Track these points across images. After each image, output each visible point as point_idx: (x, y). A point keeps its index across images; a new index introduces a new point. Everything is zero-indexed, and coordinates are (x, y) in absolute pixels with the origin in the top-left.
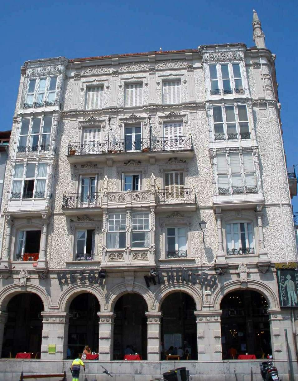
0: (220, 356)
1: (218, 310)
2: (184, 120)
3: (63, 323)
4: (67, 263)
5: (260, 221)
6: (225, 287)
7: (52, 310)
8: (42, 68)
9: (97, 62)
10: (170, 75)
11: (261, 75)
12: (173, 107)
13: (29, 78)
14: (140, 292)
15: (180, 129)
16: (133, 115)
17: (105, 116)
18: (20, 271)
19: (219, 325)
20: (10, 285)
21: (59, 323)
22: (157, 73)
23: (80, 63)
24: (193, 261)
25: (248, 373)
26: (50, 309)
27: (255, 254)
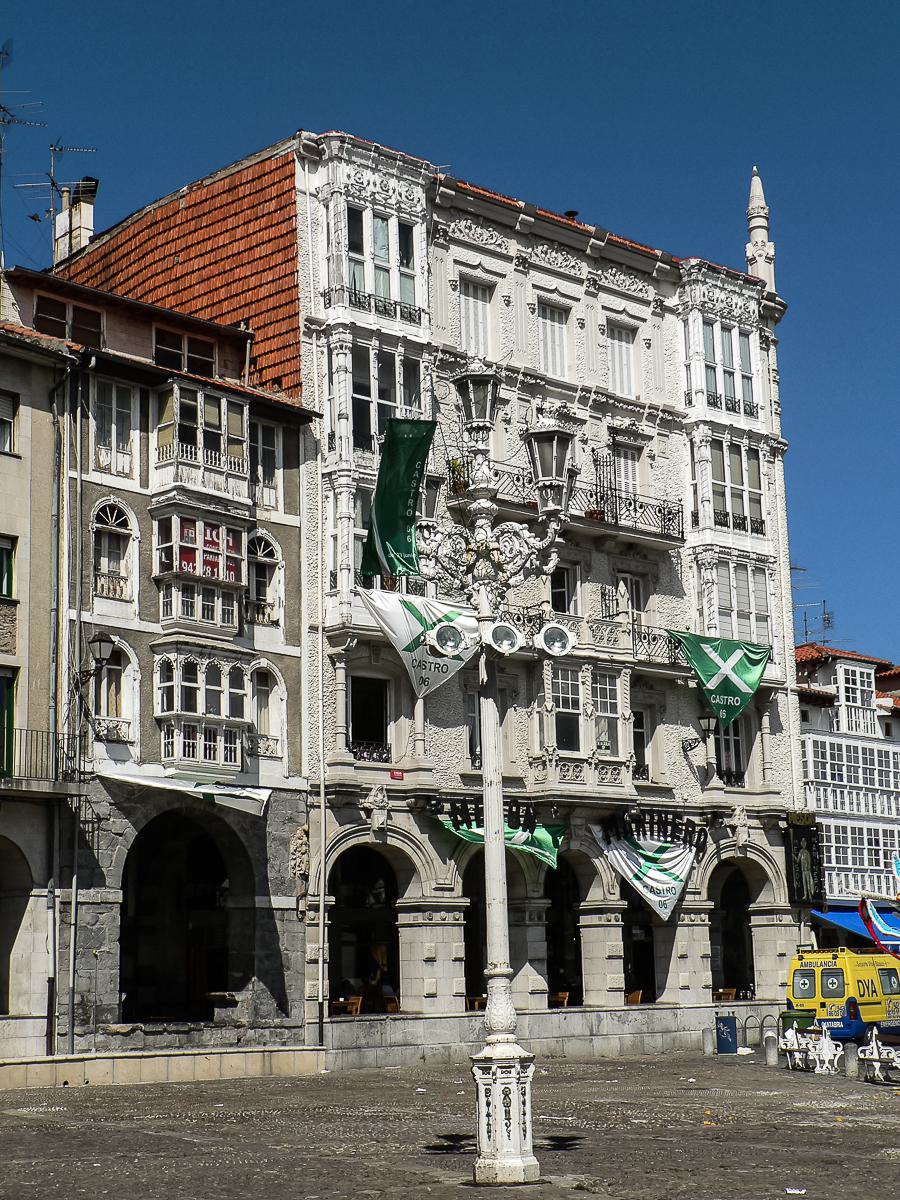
0: (461, 1002)
1: (458, 897)
2: (579, 434)
3: (460, 925)
4: (463, 776)
5: (766, 721)
6: (723, 848)
7: (439, 893)
8: (376, 178)
9: (488, 209)
10: (475, 267)
11: (582, 326)
12: (630, 407)
13: (350, 198)
14: (590, 854)
15: (634, 465)
16: (565, 407)
17: (509, 388)
18: (370, 789)
19: (459, 932)
20: (349, 826)
21: (454, 925)
22: (602, 295)
23: (531, 222)
24: (668, 792)
25: (348, 1044)
26: (436, 889)
27: (747, 787)
